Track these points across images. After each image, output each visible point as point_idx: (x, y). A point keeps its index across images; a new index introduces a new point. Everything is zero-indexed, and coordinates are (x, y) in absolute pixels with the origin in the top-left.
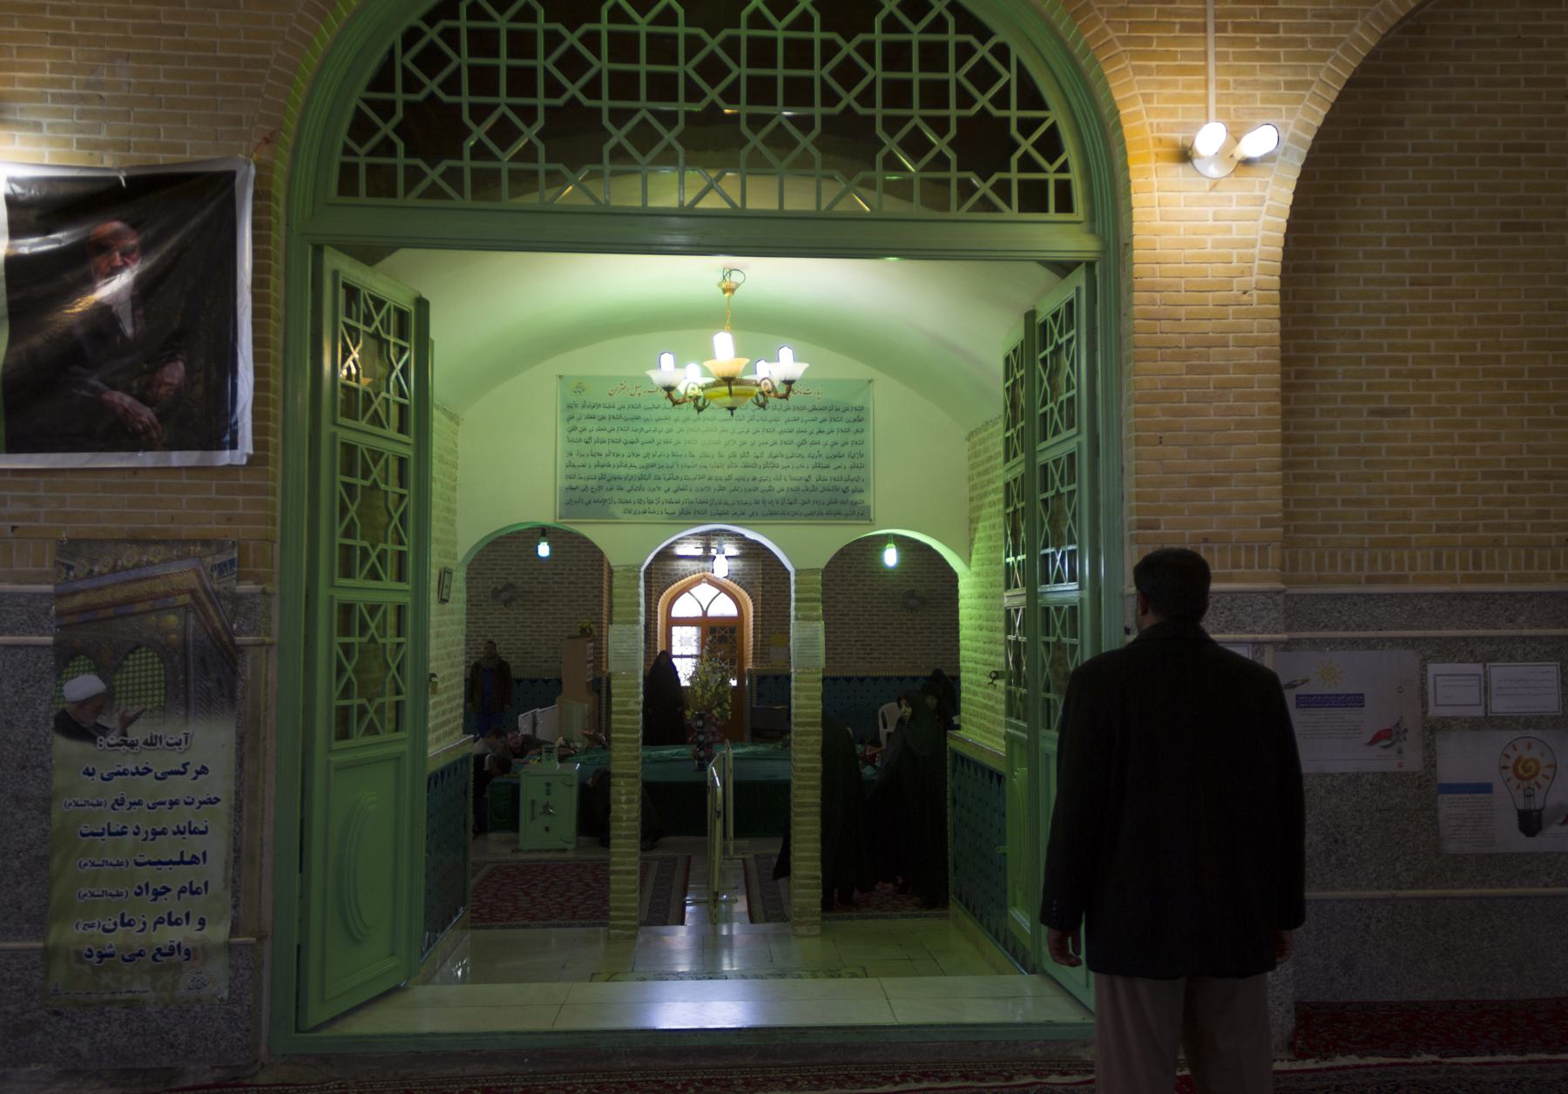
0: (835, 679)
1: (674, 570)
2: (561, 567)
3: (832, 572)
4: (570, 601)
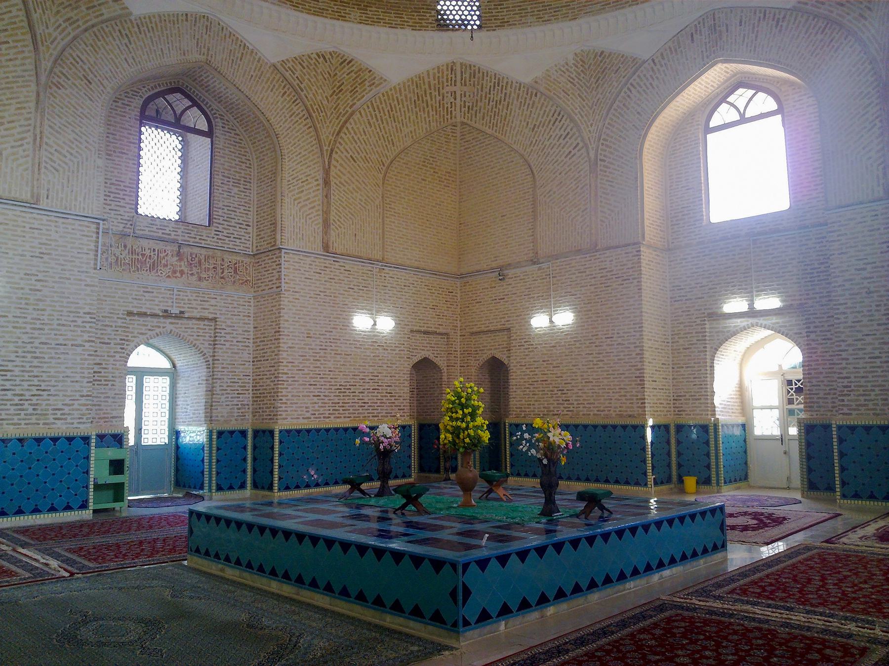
0: (853, 428)
1: (725, 327)
2: (610, 332)
3: (859, 312)
4: (619, 359)
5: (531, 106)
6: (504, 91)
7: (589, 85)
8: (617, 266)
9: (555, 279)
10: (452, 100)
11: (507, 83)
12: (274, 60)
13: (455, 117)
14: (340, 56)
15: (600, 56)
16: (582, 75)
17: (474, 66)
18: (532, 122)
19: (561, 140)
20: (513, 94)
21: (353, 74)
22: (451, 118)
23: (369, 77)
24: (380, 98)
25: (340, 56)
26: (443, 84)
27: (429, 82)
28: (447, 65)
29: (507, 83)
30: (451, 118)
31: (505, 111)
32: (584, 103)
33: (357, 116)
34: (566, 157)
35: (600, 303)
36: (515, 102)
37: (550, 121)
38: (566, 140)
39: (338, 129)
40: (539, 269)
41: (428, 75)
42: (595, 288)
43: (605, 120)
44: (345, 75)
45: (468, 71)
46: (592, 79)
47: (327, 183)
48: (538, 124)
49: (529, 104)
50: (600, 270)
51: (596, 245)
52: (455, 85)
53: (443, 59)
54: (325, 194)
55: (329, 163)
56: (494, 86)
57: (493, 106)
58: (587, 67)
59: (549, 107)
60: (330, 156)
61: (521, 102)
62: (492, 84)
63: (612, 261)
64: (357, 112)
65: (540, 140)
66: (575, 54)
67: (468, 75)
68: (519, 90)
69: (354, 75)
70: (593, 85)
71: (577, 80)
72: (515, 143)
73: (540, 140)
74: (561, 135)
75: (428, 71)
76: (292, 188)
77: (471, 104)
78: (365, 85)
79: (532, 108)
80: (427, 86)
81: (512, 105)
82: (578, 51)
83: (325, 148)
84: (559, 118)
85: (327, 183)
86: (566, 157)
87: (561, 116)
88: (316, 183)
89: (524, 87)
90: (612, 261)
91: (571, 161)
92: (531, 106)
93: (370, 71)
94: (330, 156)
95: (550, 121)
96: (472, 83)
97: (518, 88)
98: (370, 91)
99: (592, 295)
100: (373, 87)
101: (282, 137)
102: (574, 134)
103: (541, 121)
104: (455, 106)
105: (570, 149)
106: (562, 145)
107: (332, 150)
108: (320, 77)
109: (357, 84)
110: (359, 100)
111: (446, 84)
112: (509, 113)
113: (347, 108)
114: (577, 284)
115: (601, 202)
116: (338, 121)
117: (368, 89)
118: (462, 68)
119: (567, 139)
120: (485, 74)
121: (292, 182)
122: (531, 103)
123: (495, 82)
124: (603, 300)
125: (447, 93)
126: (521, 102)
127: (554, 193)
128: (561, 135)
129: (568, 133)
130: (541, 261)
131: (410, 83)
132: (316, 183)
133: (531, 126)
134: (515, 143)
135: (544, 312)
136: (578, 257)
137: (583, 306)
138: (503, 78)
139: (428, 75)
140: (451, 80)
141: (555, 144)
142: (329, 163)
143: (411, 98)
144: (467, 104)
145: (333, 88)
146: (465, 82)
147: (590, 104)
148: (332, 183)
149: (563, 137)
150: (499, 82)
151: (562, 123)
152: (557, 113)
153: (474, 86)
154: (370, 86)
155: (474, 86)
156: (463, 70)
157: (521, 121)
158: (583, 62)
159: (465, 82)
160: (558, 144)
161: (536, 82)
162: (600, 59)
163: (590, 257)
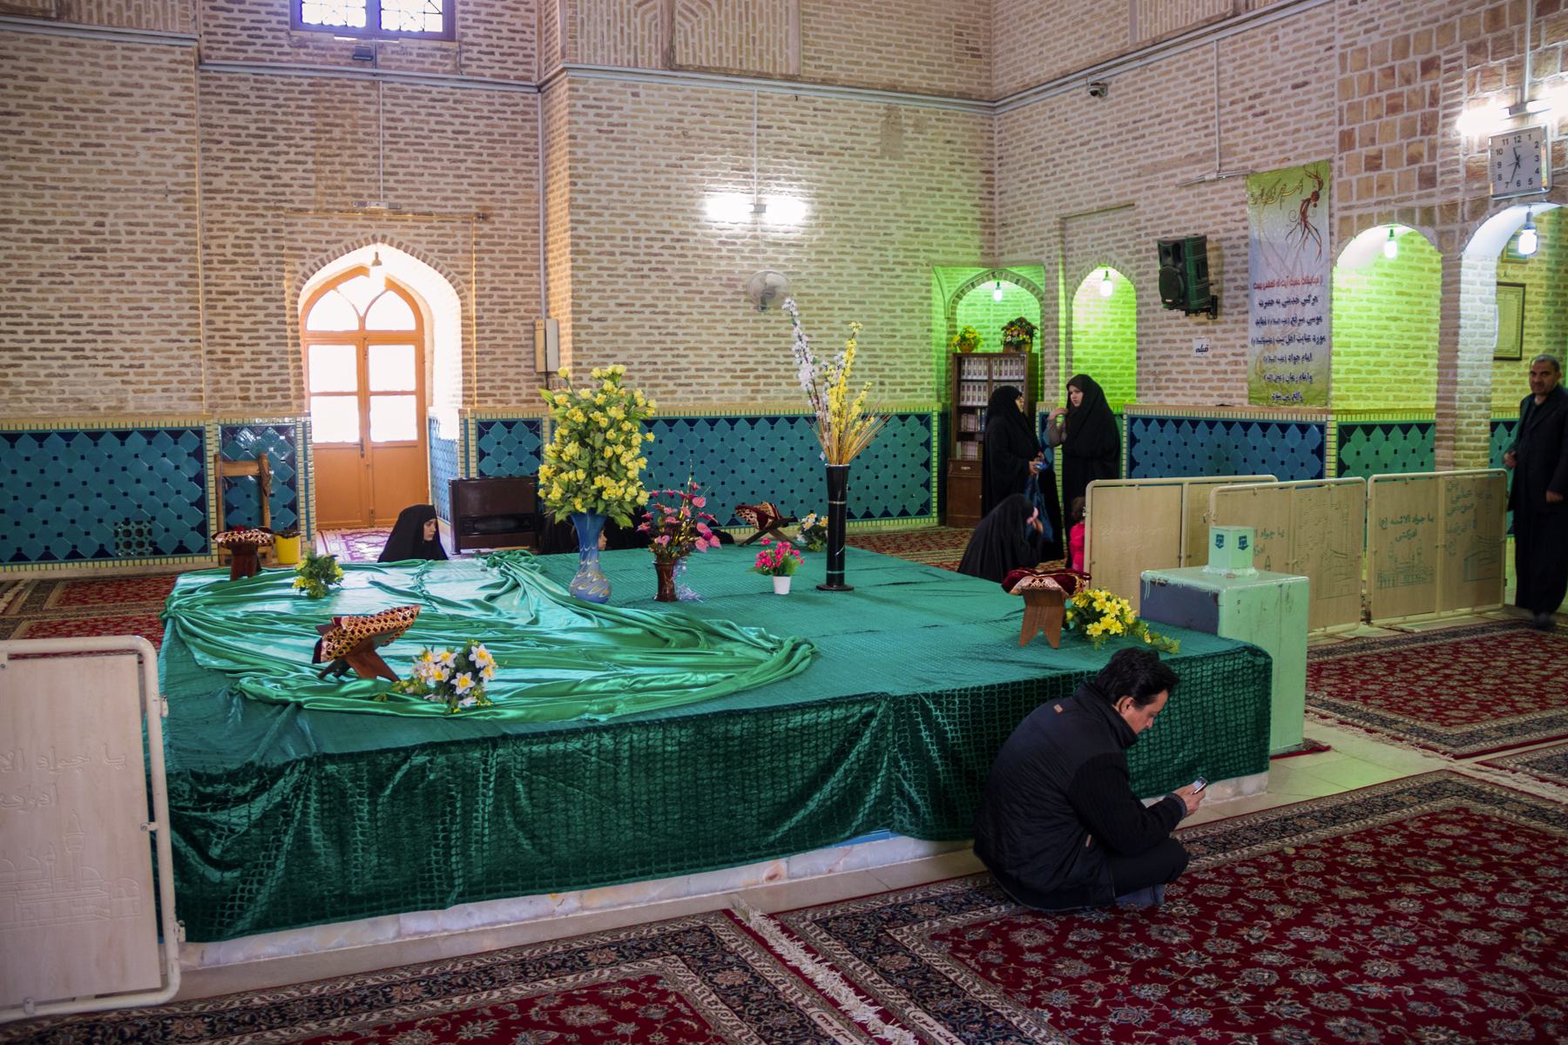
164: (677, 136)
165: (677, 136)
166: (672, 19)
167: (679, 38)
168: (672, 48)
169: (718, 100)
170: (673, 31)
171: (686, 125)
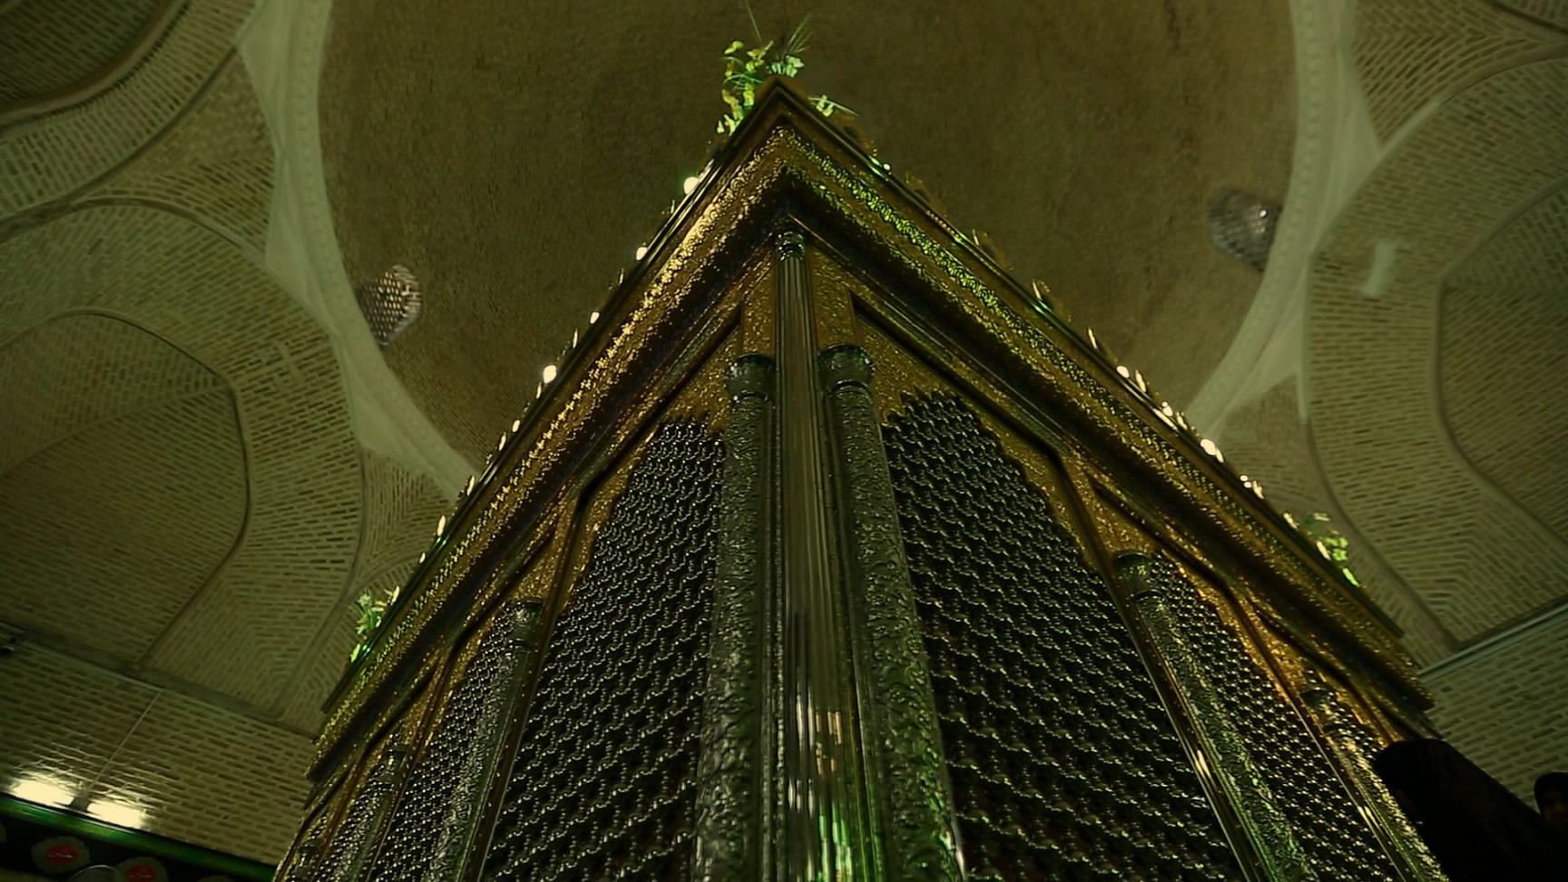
5: (333, 469)
6: (327, 424)
7: (405, 513)
8: (294, 768)
9: (148, 725)
10: (265, 361)
11: (342, 421)
12: (244, 51)
13: (235, 377)
14: (269, 165)
15: (441, 502)
16: (409, 499)
17: (337, 367)
18: (312, 485)
19: (323, 538)
20: (330, 437)
21: (251, 194)
22: (231, 372)
23: (258, 223)
24: (230, 251)
25: (269, 165)
26: (287, 337)
27: (283, 317)
28: (320, 331)
29: (342, 421)
30: (231, 372)
31: (298, 441)
32: (387, 527)
33: (183, 224)
34: (312, 562)
35: (220, 819)
36: (323, 447)
37: (335, 505)
38: (330, 543)
39: (152, 198)
40: (125, 687)
41: (296, 311)
42: (229, 786)
43: (393, 564)
44: (243, 181)
45: (324, 363)
46: (413, 513)
47: (43, 215)
48: (316, 493)
49: (333, 465)
50: (259, 758)
51: (281, 714)
52: (292, 354)
53: (327, 320)
54: (19, 221)
55: (82, 206)
56: (326, 407)
57: (294, 420)
58: (420, 497)
59: (350, 492)
60: (98, 203)
61: (328, 454)
62: (326, 403)
63: (290, 754)
64: (191, 223)
65: (296, 513)
66: (423, 476)
67: (317, 364)
68: (345, 442)
69: (248, 196)
70: (409, 520)
71: (400, 498)
72: (259, 482)
73: (296, 513)
74: (330, 533)
75: (301, 309)
76: (19, 147)
77: (273, 389)
78: (242, 220)
79: (333, 472)
80: (275, 316)
81: (315, 445)
82: (429, 476)
83: (107, 186)
84: (348, 514)
85: (43, 215)
86: (312, 562)
87: (353, 513)
88: (34, 192)
89: (352, 445)
90: (290, 754)
91: (316, 572)
92: (333, 469)
93: (266, 221)
94: (98, 203)
95: (335, 505)
96: (310, 375)
97: (345, 438)
98: (237, 232)
99: (214, 795)
100: (246, 235)
101: (120, 96)
102: (348, 546)
103: (322, 496)
104: (255, 370)
105: (328, 558)
106: (319, 544)
107: (108, 202)
108: (226, 138)
109: (237, 206)
110: (216, 219)
111: (288, 341)
112: (299, 447)
113: (194, 205)
114: (193, 759)
115: (324, 656)
116: (164, 193)
117: (239, 229)
118: (324, 351)
119: (333, 544)
120: (334, 387)
121: (34, 141)
122: (337, 467)
123: (331, 405)
124: (231, 815)
125: (276, 348)
126: (328, 454)
127: (258, 591)
128: (330, 533)
129: (341, 539)
130: (144, 675)
131: (272, 290)
132: (34, 192)
133: (305, 487)
134: (259, 482)
135: (67, 777)
136: (228, 714)
137: (178, 806)
138: (346, 413)
139: (296, 311)
140: (298, 345)
141: (310, 535)
142: (82, 206)
143: (244, 300)
144: (269, 384)
145: (215, 166)
146: (305, 365)
147: (391, 534)
148: (42, 229)
149: (330, 537)
150: (336, 411)
151: (345, 521)
152: (352, 506)
153: (308, 380)
154: (245, 229)
155: (308, 380)
156: (322, 355)
157: (301, 470)
158: (422, 489)
159: (305, 365)
160: (316, 538)
161: (369, 456)
162: (438, 504)
163: (254, 726)
164: (1521, 704)
165: (1521, 704)
166: (1428, 612)
167: (1447, 622)
168: (1447, 633)
169: (1537, 649)
170: (1435, 620)
171: (1522, 689)
